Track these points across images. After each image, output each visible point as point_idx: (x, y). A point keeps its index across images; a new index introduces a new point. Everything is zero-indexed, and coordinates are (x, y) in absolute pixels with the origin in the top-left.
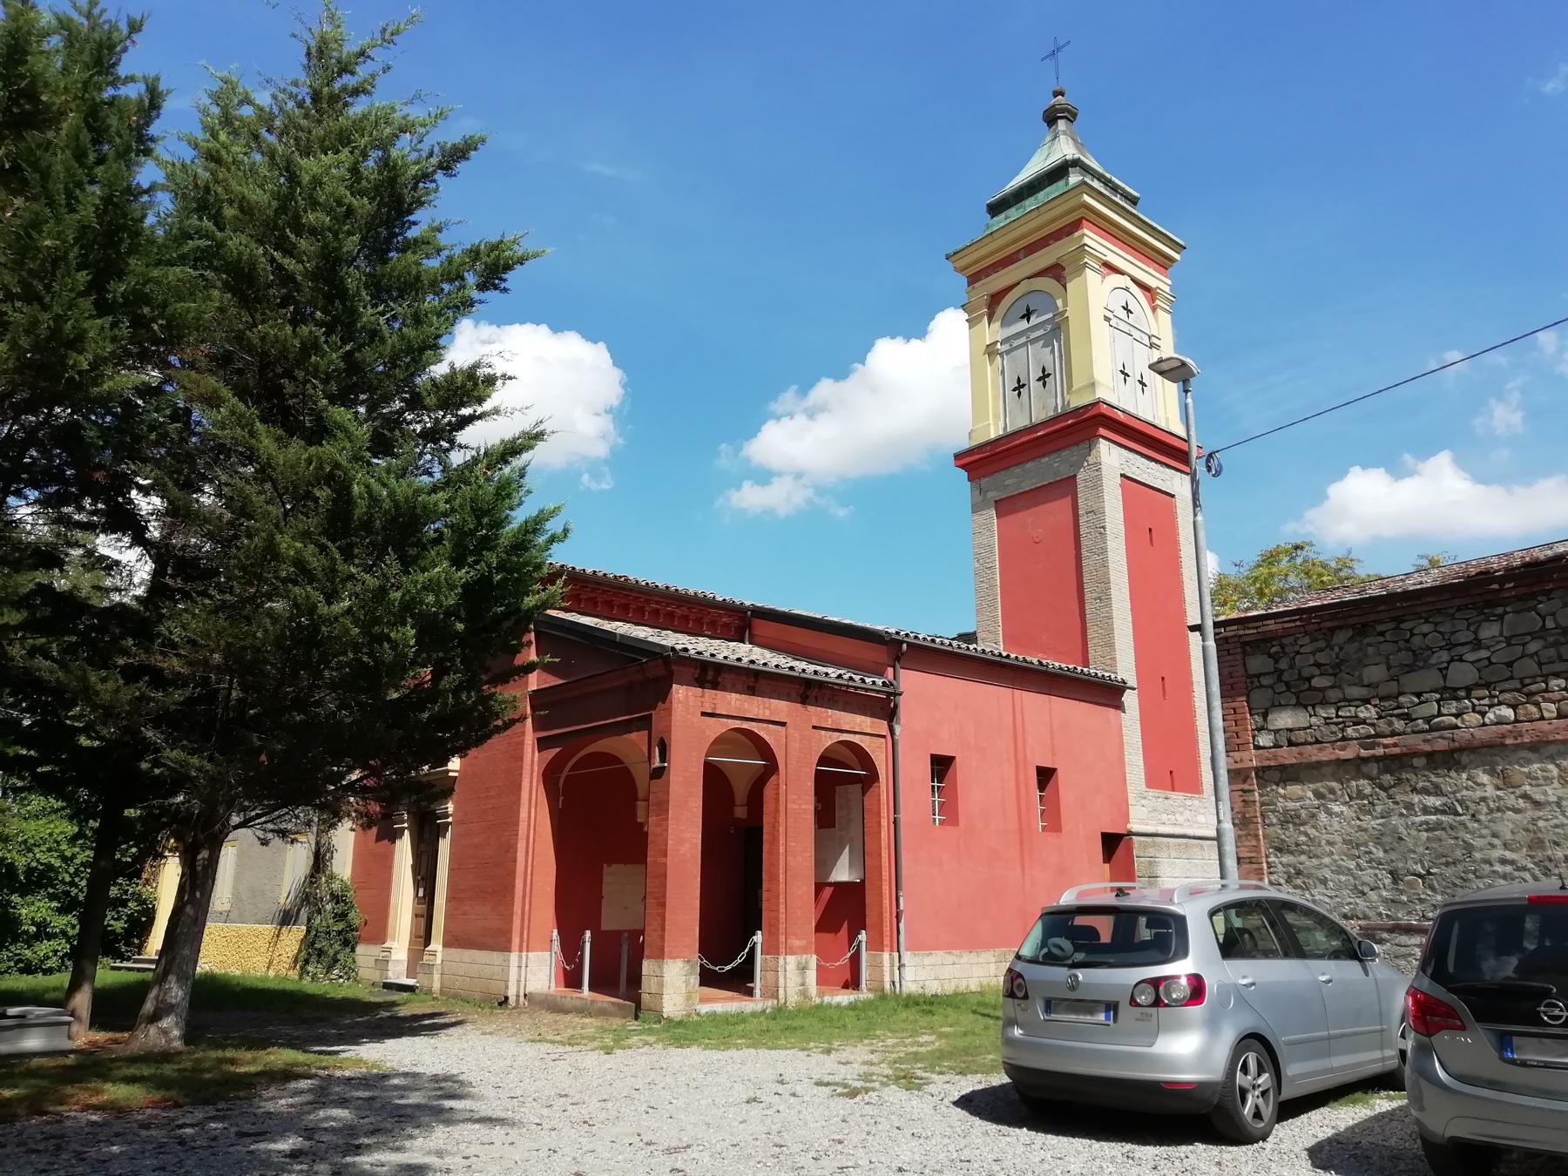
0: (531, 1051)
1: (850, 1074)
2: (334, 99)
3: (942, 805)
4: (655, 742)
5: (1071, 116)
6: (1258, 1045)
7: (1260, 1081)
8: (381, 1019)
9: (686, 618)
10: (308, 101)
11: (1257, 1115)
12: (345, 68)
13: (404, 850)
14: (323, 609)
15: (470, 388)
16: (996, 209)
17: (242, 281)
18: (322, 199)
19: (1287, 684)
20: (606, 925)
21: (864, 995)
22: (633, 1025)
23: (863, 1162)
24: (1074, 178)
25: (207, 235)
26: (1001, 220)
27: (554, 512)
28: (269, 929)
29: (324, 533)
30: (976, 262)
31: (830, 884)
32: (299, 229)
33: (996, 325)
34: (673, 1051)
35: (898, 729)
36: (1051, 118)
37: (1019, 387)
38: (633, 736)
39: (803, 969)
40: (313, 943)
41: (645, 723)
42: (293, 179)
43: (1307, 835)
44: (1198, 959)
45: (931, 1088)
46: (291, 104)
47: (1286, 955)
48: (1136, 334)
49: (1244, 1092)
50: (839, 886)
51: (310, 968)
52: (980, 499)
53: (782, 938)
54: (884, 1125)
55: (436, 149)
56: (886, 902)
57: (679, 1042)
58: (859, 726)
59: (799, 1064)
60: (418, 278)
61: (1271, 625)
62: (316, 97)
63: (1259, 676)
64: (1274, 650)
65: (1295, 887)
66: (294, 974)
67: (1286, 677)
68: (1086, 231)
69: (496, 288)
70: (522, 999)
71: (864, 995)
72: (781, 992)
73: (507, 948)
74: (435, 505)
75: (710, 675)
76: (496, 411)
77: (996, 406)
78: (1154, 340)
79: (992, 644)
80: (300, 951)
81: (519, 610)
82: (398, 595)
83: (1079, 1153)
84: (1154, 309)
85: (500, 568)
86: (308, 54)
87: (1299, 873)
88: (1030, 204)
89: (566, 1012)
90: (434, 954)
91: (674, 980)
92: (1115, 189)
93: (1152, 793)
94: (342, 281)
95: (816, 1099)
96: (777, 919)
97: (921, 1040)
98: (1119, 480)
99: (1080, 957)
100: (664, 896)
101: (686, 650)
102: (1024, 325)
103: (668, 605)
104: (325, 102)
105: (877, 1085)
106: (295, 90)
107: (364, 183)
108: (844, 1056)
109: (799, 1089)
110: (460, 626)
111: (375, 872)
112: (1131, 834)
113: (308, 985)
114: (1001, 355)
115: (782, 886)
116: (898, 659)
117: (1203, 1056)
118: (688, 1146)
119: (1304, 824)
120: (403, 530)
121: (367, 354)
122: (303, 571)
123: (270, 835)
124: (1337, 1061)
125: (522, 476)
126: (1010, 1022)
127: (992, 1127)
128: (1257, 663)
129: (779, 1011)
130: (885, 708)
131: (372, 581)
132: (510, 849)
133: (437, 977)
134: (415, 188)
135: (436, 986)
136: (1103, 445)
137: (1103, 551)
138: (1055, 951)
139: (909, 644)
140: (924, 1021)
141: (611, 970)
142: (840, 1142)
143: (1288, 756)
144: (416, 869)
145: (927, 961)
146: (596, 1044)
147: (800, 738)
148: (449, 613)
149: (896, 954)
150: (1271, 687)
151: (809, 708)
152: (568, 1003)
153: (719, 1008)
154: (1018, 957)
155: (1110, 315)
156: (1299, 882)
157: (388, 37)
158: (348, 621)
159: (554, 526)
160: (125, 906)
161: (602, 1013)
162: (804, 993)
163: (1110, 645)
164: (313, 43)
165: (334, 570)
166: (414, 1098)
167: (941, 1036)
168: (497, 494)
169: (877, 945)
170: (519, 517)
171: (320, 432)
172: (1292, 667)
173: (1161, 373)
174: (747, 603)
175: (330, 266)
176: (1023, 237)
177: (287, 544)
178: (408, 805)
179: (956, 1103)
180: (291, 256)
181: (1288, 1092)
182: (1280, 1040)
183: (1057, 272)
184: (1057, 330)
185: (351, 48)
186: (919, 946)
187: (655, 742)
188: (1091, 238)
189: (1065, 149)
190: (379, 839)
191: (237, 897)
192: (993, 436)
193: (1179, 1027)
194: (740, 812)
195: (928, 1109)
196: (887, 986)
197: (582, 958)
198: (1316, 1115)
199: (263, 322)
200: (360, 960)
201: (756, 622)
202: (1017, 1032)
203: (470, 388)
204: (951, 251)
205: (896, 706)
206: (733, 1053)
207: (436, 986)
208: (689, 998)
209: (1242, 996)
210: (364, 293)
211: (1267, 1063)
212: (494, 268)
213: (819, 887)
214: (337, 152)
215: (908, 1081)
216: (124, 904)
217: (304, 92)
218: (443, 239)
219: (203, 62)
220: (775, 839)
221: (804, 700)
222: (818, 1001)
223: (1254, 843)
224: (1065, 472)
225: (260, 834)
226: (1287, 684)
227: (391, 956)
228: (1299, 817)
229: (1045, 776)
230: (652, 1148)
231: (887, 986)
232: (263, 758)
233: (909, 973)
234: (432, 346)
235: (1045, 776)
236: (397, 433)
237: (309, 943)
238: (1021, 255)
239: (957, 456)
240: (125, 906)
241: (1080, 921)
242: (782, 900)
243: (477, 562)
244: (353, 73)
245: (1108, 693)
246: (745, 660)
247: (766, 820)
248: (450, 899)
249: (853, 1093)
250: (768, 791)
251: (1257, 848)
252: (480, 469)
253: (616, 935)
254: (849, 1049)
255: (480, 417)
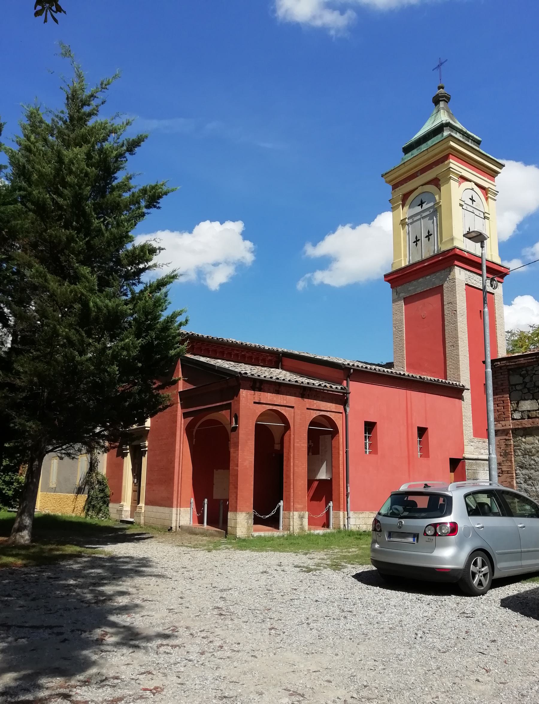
0: (176, 549)
1: (310, 563)
2: (80, 119)
3: (370, 445)
4: (233, 415)
5: (447, 99)
6: (483, 554)
7: (483, 570)
8: (118, 535)
9: (251, 358)
10: (68, 121)
11: (480, 583)
12: (85, 103)
13: (128, 462)
14: (78, 358)
15: (147, 252)
16: (407, 150)
17: (41, 209)
18: (74, 169)
19: (528, 389)
20: (215, 497)
21: (330, 530)
22: (224, 540)
23: (302, 598)
24: (446, 133)
25: (24, 190)
26: (409, 156)
27: (180, 314)
28: (72, 496)
29: (79, 324)
30: (396, 178)
31: (317, 480)
32: (65, 184)
33: (406, 208)
34: (238, 552)
35: (348, 410)
36: (436, 101)
37: (417, 241)
38: (224, 412)
39: (301, 518)
40: (91, 502)
41: (228, 407)
42: (60, 161)
43: (535, 461)
44: (457, 515)
45: (345, 570)
46: (61, 123)
47: (504, 515)
48: (477, 212)
49: (474, 574)
50: (321, 481)
51: (90, 513)
52: (397, 297)
53: (292, 504)
54: (318, 583)
55: (125, 142)
56: (342, 489)
57: (241, 548)
58: (329, 408)
59: (289, 558)
60: (118, 204)
61: (522, 361)
62: (71, 118)
63: (515, 385)
64: (523, 372)
65: (528, 485)
66: (83, 515)
67: (528, 386)
68: (451, 160)
69: (155, 206)
70: (178, 528)
71: (330, 530)
72: (291, 528)
73: (171, 506)
74: (126, 311)
75: (258, 385)
76: (155, 265)
77: (405, 251)
78: (486, 215)
79: (401, 369)
80: (85, 505)
81: (167, 356)
82: (111, 351)
83: (397, 597)
84: (487, 199)
85: (156, 339)
86: (68, 98)
87: (530, 478)
88: (424, 147)
89: (196, 534)
90: (141, 508)
91: (242, 521)
92: (468, 137)
93: (476, 439)
94: (84, 208)
95: (292, 573)
96: (290, 495)
97: (351, 550)
98: (464, 287)
99: (406, 514)
100: (237, 485)
101: (246, 373)
102: (418, 209)
103: (242, 351)
104: (77, 120)
105: (322, 568)
106: (62, 115)
107: (93, 160)
108: (312, 556)
109: (286, 568)
110: (140, 365)
111: (116, 470)
112: (465, 459)
113: (88, 520)
114: (408, 225)
115: (292, 481)
116: (349, 376)
117: (455, 558)
118: (230, 589)
119: (533, 456)
120: (113, 323)
121: (96, 241)
122: (70, 343)
123: (63, 456)
124: (525, 563)
125: (166, 296)
126: (374, 542)
127: (364, 586)
128: (516, 379)
129: (291, 536)
130: (342, 399)
131: (99, 346)
132: (172, 462)
133: (142, 518)
134: (116, 161)
135: (142, 522)
136: (457, 270)
137: (455, 322)
138: (396, 511)
139: (354, 370)
140: (355, 542)
141: (216, 516)
142: (295, 590)
143: (527, 423)
144: (133, 470)
145: (361, 516)
146: (205, 548)
147: (300, 414)
148: (134, 358)
149: (346, 513)
150: (521, 390)
151: (305, 400)
152: (197, 531)
153: (262, 534)
154: (379, 514)
155: (462, 203)
156: (530, 482)
157: (104, 86)
158: (89, 364)
159: (180, 319)
160: (13, 485)
161: (211, 535)
162: (302, 529)
163: (458, 368)
164: (70, 92)
165: (83, 341)
166: (129, 567)
167: (361, 549)
168: (154, 305)
169: (337, 508)
170: (165, 315)
171: (76, 279)
172: (531, 381)
173: (470, 238)
174: (280, 350)
175: (78, 200)
176: (420, 164)
177: (63, 330)
178: (129, 442)
179: (353, 576)
180: (62, 197)
181: (497, 575)
182: (495, 552)
183: (436, 182)
184: (436, 211)
185: (87, 93)
186: (356, 509)
187: (233, 415)
188: (454, 164)
189: (443, 117)
190: (118, 456)
191: (58, 482)
192: (403, 265)
193: (446, 545)
194: (277, 447)
195: (340, 578)
196: (342, 526)
197: (203, 511)
198: (512, 586)
199: (51, 228)
200: (111, 510)
201: (284, 359)
202: (377, 546)
203: (147, 252)
204: (384, 173)
205: (347, 399)
206: (264, 554)
207: (142, 522)
208: (248, 529)
209: (476, 532)
210: (93, 214)
211: (487, 561)
212: (153, 197)
213: (310, 482)
214: (81, 147)
215: (336, 567)
216: (12, 484)
217: (66, 116)
218: (132, 183)
219: (21, 104)
220: (289, 459)
221: (303, 396)
222: (309, 532)
223: (510, 464)
224: (438, 283)
225: (59, 455)
226: (528, 389)
227: (124, 508)
228: (531, 452)
229: (422, 431)
230: (215, 589)
231: (342, 526)
232: (56, 422)
233: (352, 521)
234: (126, 238)
235: (422, 431)
236: (111, 277)
237: (89, 502)
238: (419, 174)
239: (386, 276)
240: (13, 485)
241: (411, 498)
242: (292, 487)
243: (146, 336)
244: (89, 105)
245: (456, 392)
246: (274, 378)
247: (285, 450)
248: (147, 484)
249: (309, 570)
250: (286, 438)
251: (511, 466)
252: (147, 293)
253: (218, 501)
254: (316, 553)
255: (149, 268)
